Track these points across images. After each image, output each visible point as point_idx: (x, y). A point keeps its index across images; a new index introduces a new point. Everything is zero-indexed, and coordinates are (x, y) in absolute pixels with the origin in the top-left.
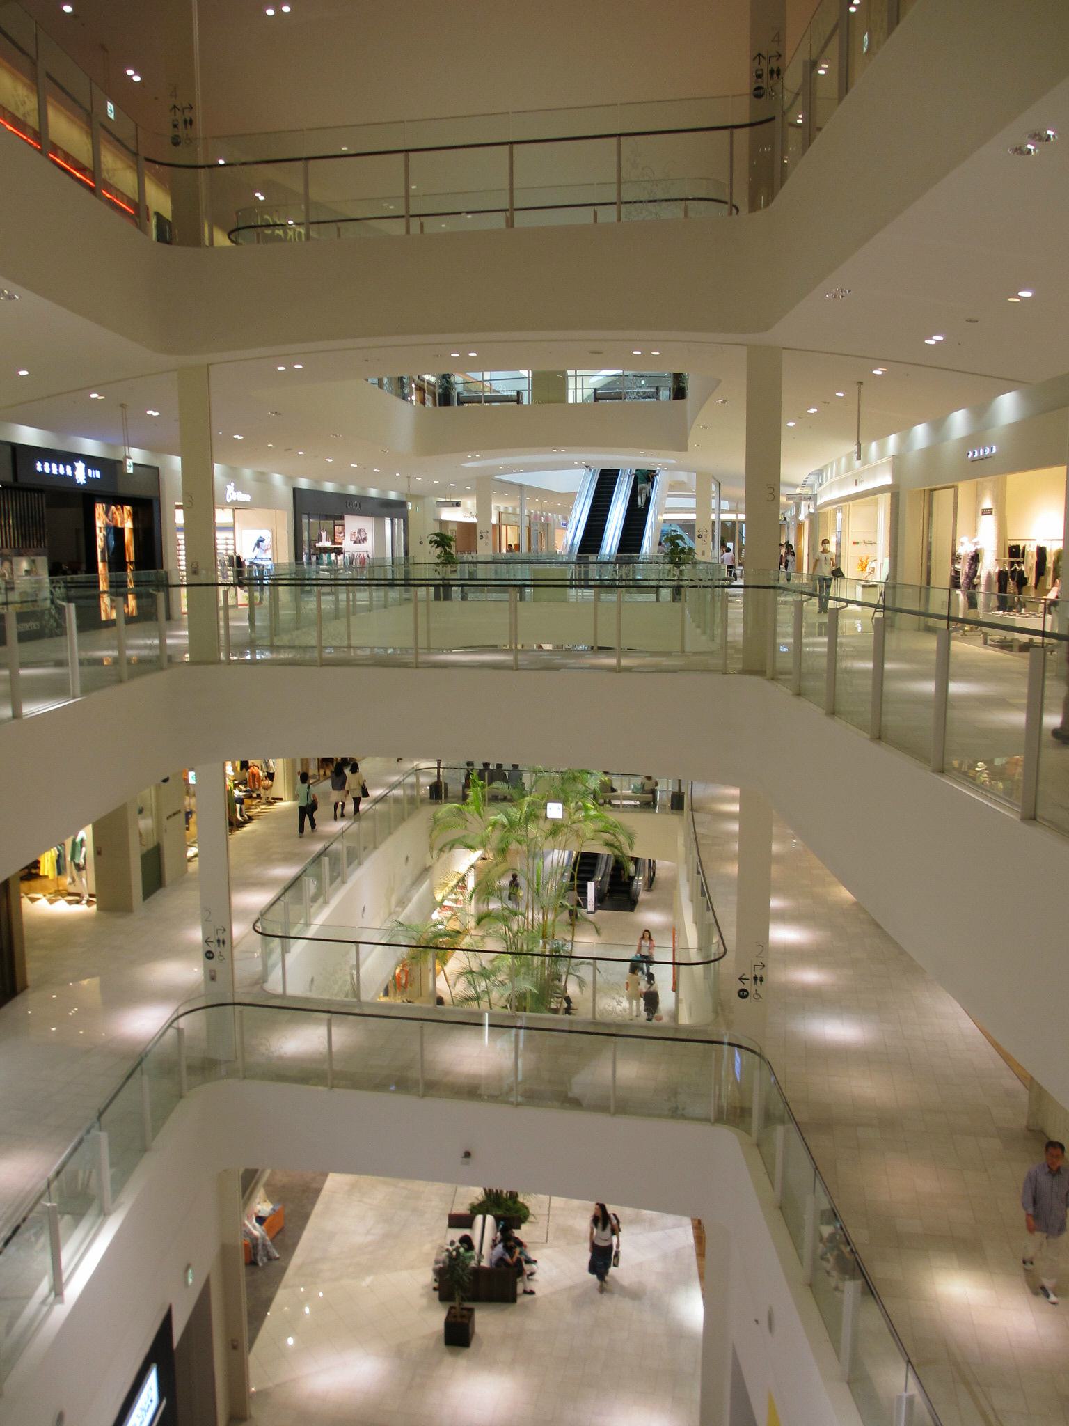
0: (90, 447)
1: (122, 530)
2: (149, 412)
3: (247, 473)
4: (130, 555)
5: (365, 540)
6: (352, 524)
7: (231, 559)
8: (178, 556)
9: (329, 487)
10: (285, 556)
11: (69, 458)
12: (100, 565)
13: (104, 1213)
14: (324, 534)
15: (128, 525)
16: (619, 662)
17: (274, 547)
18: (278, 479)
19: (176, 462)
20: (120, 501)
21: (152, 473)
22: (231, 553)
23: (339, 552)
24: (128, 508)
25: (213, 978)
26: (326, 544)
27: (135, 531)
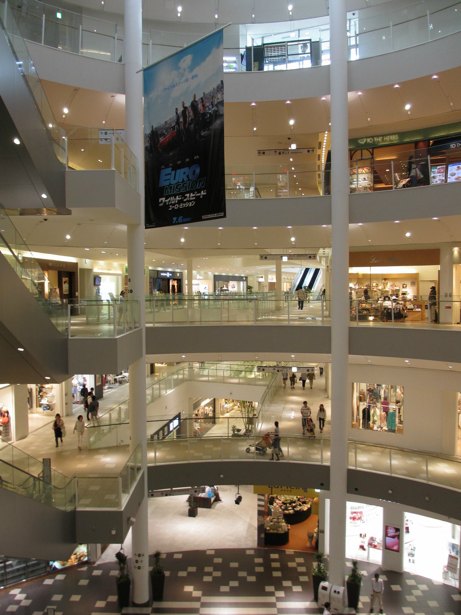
0: (170, 270)
1: (175, 286)
2: (102, 252)
3: (202, 272)
4: (176, 291)
5: (235, 287)
6: (231, 283)
7: (198, 292)
8: (186, 290)
9: (224, 274)
10: (211, 291)
11: (166, 272)
12: (170, 293)
13: (172, 389)
14: (225, 286)
15: (176, 285)
16: (289, 323)
17: (208, 289)
18: (210, 273)
19: (186, 271)
20: (174, 280)
21: (181, 274)
22: (198, 291)
23: (228, 290)
24: (176, 281)
25: (189, 365)
26: (225, 288)
27: (177, 286)
